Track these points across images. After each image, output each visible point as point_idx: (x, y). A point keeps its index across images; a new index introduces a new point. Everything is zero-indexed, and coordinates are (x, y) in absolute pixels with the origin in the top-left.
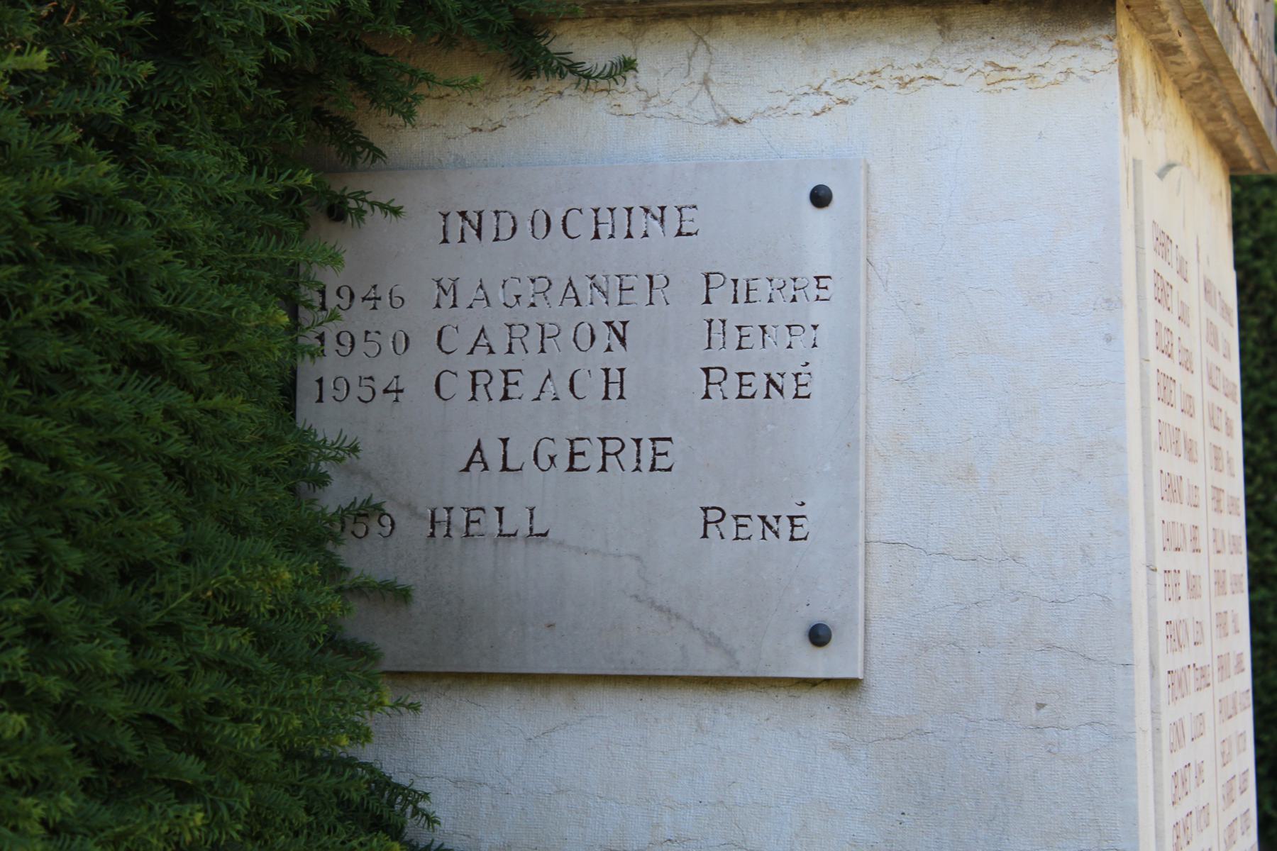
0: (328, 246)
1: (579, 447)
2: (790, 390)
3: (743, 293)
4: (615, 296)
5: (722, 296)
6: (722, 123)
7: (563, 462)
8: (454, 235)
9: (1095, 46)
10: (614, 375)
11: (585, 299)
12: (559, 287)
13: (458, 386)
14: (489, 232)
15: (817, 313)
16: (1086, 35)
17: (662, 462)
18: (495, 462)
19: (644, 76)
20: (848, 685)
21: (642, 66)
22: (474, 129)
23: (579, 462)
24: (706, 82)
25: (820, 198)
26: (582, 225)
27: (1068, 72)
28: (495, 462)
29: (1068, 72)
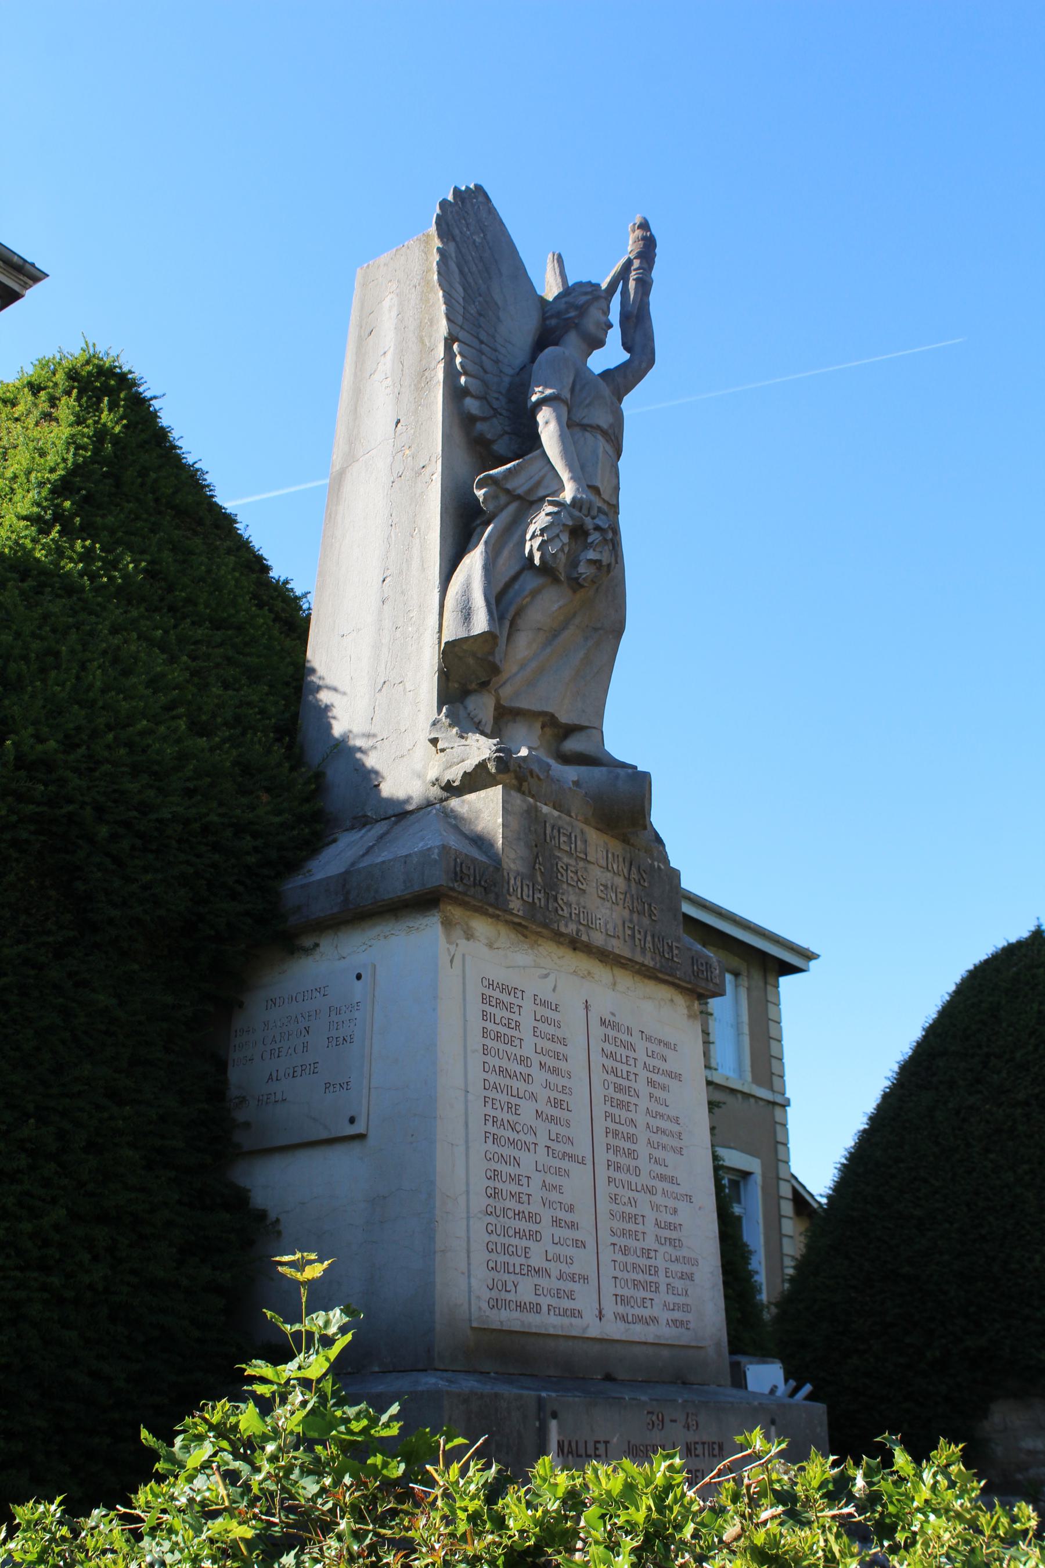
0: (570, 1456)
1: (556, 1240)
2: (349, 1041)
3: (339, 1012)
4: (307, 1019)
5: (333, 1013)
6: (339, 959)
7: (291, 1075)
8: (269, 1007)
9: (434, 916)
10: (305, 1044)
11: (300, 1021)
12: (294, 1018)
13: (267, 1055)
14: (277, 1005)
15: (357, 1014)
16: (432, 912)
17: (316, 1070)
18: (274, 1078)
19: (322, 949)
20: (361, 1137)
21: (321, 945)
22: (398, 422)
23: (295, 1075)
24: (336, 947)
25: (359, 977)
26: (300, 998)
27: (427, 925)
28: (274, 1078)
29: (427, 925)
